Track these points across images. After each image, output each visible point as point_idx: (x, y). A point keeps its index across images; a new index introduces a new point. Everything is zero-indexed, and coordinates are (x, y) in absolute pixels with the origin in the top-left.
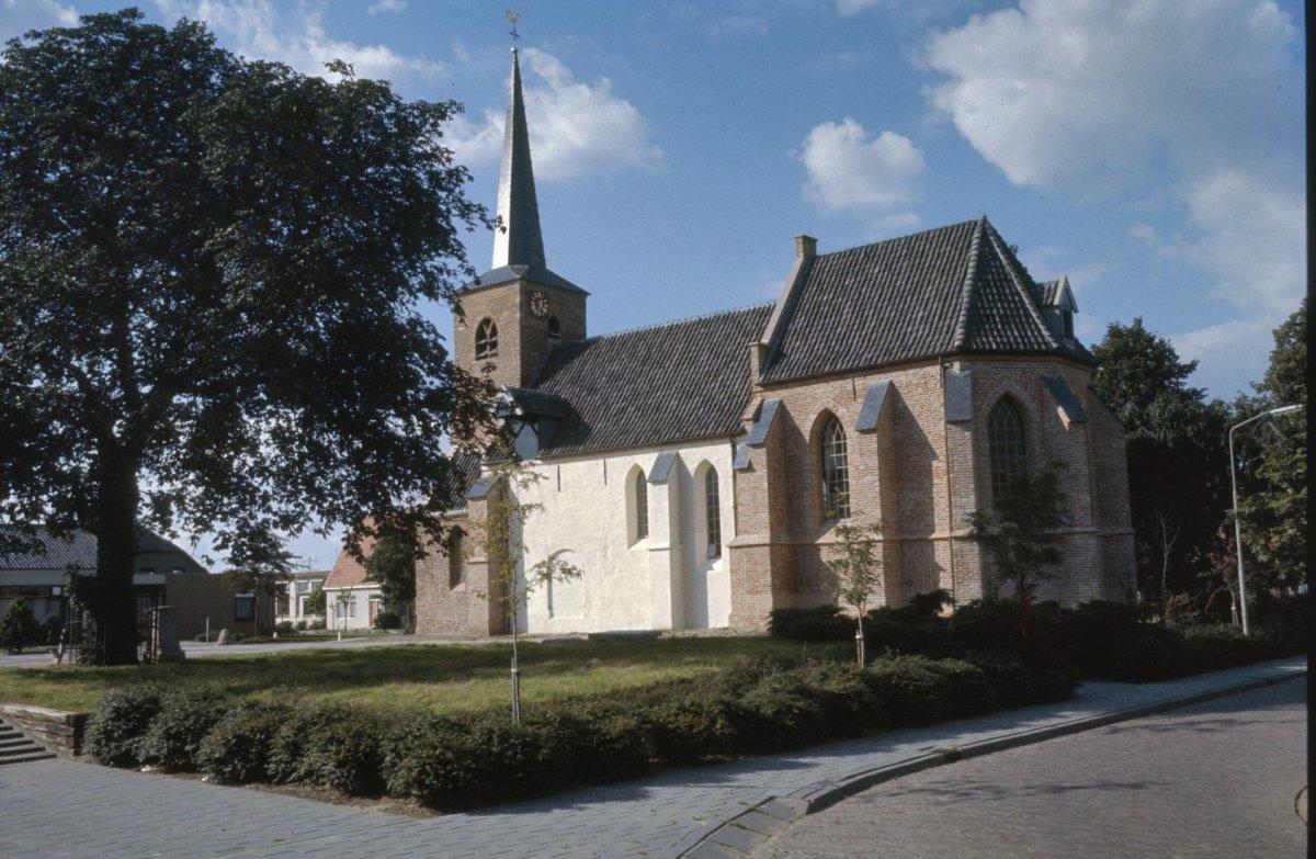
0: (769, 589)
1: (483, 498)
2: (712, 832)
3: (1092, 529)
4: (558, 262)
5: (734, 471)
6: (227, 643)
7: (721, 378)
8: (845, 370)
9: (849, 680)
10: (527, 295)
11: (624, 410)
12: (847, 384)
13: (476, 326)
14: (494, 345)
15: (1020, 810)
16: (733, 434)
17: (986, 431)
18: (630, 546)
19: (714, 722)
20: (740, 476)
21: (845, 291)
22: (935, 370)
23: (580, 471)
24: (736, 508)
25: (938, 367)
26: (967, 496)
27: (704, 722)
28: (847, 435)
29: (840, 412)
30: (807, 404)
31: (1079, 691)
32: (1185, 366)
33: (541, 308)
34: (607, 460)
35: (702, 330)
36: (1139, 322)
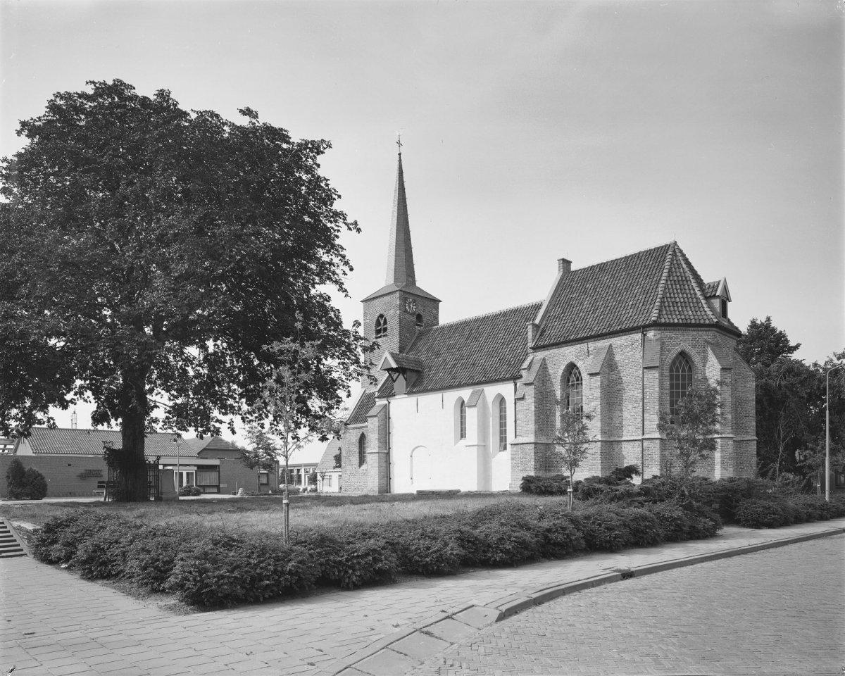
1: (375, 416)
2: (398, 640)
3: (731, 436)
4: (425, 281)
5: (515, 399)
9: (558, 519)
11: (454, 366)
12: (584, 346)
13: (375, 319)
14: (385, 330)
15: (675, 628)
16: (515, 378)
17: (668, 374)
18: (455, 444)
19: (446, 545)
20: (518, 403)
22: (638, 336)
23: (429, 401)
24: (516, 421)
27: (439, 545)
30: (559, 359)
31: (719, 532)
32: (792, 347)
33: (412, 308)
36: (768, 319)
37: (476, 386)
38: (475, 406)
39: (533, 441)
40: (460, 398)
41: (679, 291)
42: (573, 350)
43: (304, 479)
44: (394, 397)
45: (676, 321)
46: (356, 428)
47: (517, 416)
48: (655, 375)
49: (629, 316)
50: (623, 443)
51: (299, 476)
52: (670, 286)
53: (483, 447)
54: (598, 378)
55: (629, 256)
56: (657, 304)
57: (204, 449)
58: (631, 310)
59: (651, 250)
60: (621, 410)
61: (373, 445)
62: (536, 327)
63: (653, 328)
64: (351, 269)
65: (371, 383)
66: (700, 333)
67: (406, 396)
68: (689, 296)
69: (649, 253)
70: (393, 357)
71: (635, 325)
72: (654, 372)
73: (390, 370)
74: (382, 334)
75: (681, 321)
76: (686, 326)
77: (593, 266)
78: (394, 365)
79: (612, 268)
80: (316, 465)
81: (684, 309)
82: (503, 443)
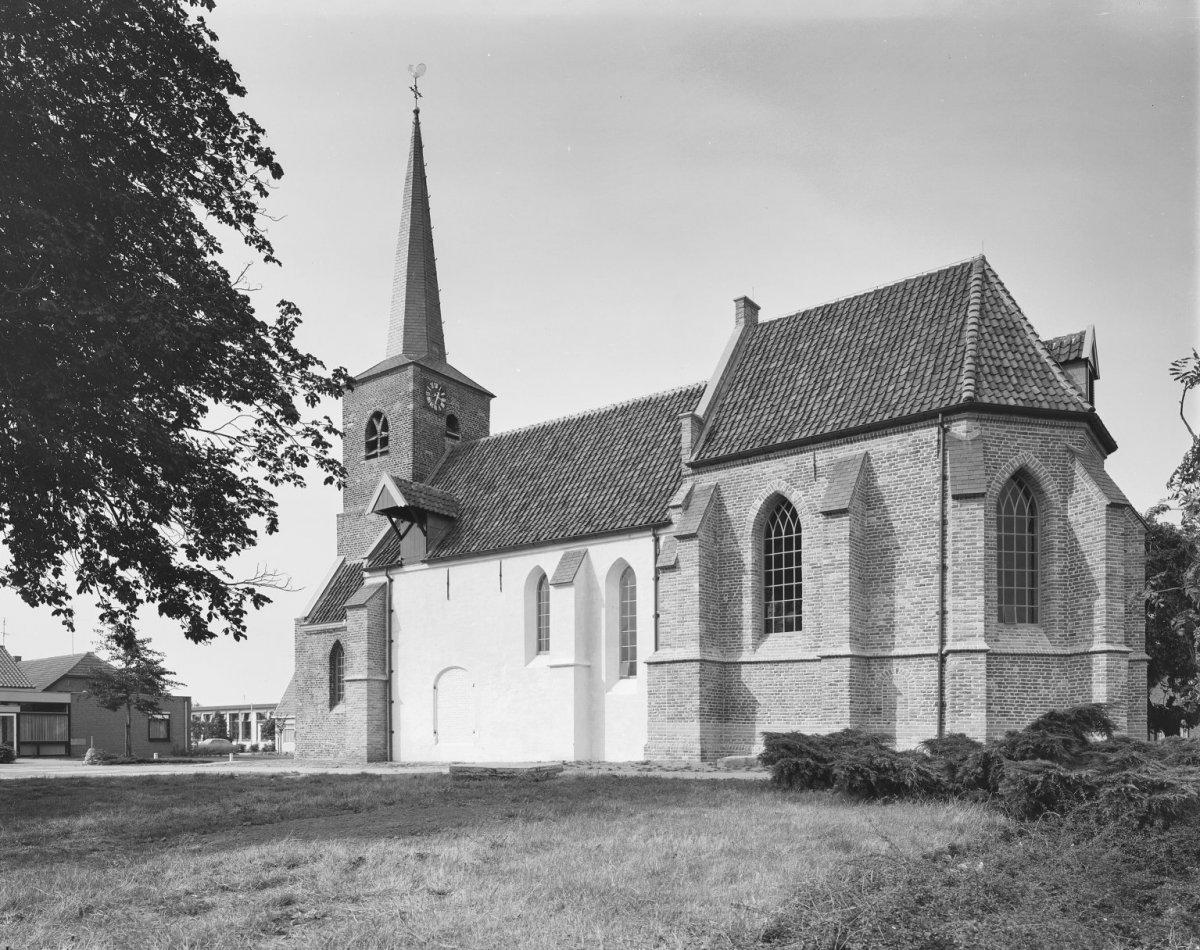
0: (696, 716)
4: (463, 355)
5: (657, 570)
6: (94, 764)
7: (641, 465)
8: (806, 438)
10: (422, 385)
11: (525, 507)
12: (806, 459)
13: (366, 420)
14: (385, 441)
16: (656, 526)
18: (527, 663)
20: (664, 577)
21: (797, 356)
22: (930, 434)
23: (474, 576)
24: (657, 616)
25: (935, 430)
26: (974, 597)
28: (803, 525)
29: (795, 497)
33: (437, 401)
34: (504, 561)
35: (618, 419)
37: (572, 545)
38: (570, 583)
39: (697, 656)
40: (538, 569)
41: (1006, 346)
42: (782, 466)
43: (256, 729)
44: (400, 570)
45: (1012, 402)
46: (324, 631)
47: (661, 605)
48: (976, 512)
49: (905, 397)
50: (895, 661)
51: (247, 726)
52: (987, 337)
53: (586, 669)
54: (845, 522)
55: (884, 290)
56: (966, 368)
57: (65, 677)
58: (908, 384)
59: (931, 276)
60: (890, 592)
61: (357, 667)
62: (698, 423)
63: (966, 415)
64: (277, 172)
65: (329, 480)
66: (1057, 432)
67: (426, 566)
68: (1027, 358)
69: (928, 281)
70: (399, 487)
71: (925, 409)
72: (974, 505)
73: (391, 512)
74: (379, 451)
75: (1020, 403)
76: (1030, 414)
77: (806, 312)
78: (401, 502)
79: (848, 312)
80: (272, 707)
81: (1023, 381)
82: (627, 663)
